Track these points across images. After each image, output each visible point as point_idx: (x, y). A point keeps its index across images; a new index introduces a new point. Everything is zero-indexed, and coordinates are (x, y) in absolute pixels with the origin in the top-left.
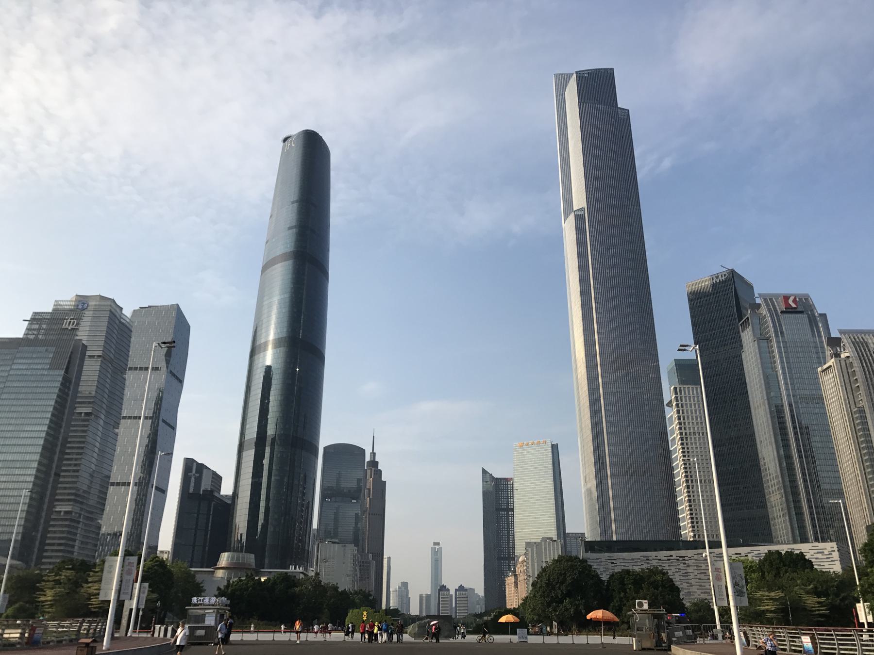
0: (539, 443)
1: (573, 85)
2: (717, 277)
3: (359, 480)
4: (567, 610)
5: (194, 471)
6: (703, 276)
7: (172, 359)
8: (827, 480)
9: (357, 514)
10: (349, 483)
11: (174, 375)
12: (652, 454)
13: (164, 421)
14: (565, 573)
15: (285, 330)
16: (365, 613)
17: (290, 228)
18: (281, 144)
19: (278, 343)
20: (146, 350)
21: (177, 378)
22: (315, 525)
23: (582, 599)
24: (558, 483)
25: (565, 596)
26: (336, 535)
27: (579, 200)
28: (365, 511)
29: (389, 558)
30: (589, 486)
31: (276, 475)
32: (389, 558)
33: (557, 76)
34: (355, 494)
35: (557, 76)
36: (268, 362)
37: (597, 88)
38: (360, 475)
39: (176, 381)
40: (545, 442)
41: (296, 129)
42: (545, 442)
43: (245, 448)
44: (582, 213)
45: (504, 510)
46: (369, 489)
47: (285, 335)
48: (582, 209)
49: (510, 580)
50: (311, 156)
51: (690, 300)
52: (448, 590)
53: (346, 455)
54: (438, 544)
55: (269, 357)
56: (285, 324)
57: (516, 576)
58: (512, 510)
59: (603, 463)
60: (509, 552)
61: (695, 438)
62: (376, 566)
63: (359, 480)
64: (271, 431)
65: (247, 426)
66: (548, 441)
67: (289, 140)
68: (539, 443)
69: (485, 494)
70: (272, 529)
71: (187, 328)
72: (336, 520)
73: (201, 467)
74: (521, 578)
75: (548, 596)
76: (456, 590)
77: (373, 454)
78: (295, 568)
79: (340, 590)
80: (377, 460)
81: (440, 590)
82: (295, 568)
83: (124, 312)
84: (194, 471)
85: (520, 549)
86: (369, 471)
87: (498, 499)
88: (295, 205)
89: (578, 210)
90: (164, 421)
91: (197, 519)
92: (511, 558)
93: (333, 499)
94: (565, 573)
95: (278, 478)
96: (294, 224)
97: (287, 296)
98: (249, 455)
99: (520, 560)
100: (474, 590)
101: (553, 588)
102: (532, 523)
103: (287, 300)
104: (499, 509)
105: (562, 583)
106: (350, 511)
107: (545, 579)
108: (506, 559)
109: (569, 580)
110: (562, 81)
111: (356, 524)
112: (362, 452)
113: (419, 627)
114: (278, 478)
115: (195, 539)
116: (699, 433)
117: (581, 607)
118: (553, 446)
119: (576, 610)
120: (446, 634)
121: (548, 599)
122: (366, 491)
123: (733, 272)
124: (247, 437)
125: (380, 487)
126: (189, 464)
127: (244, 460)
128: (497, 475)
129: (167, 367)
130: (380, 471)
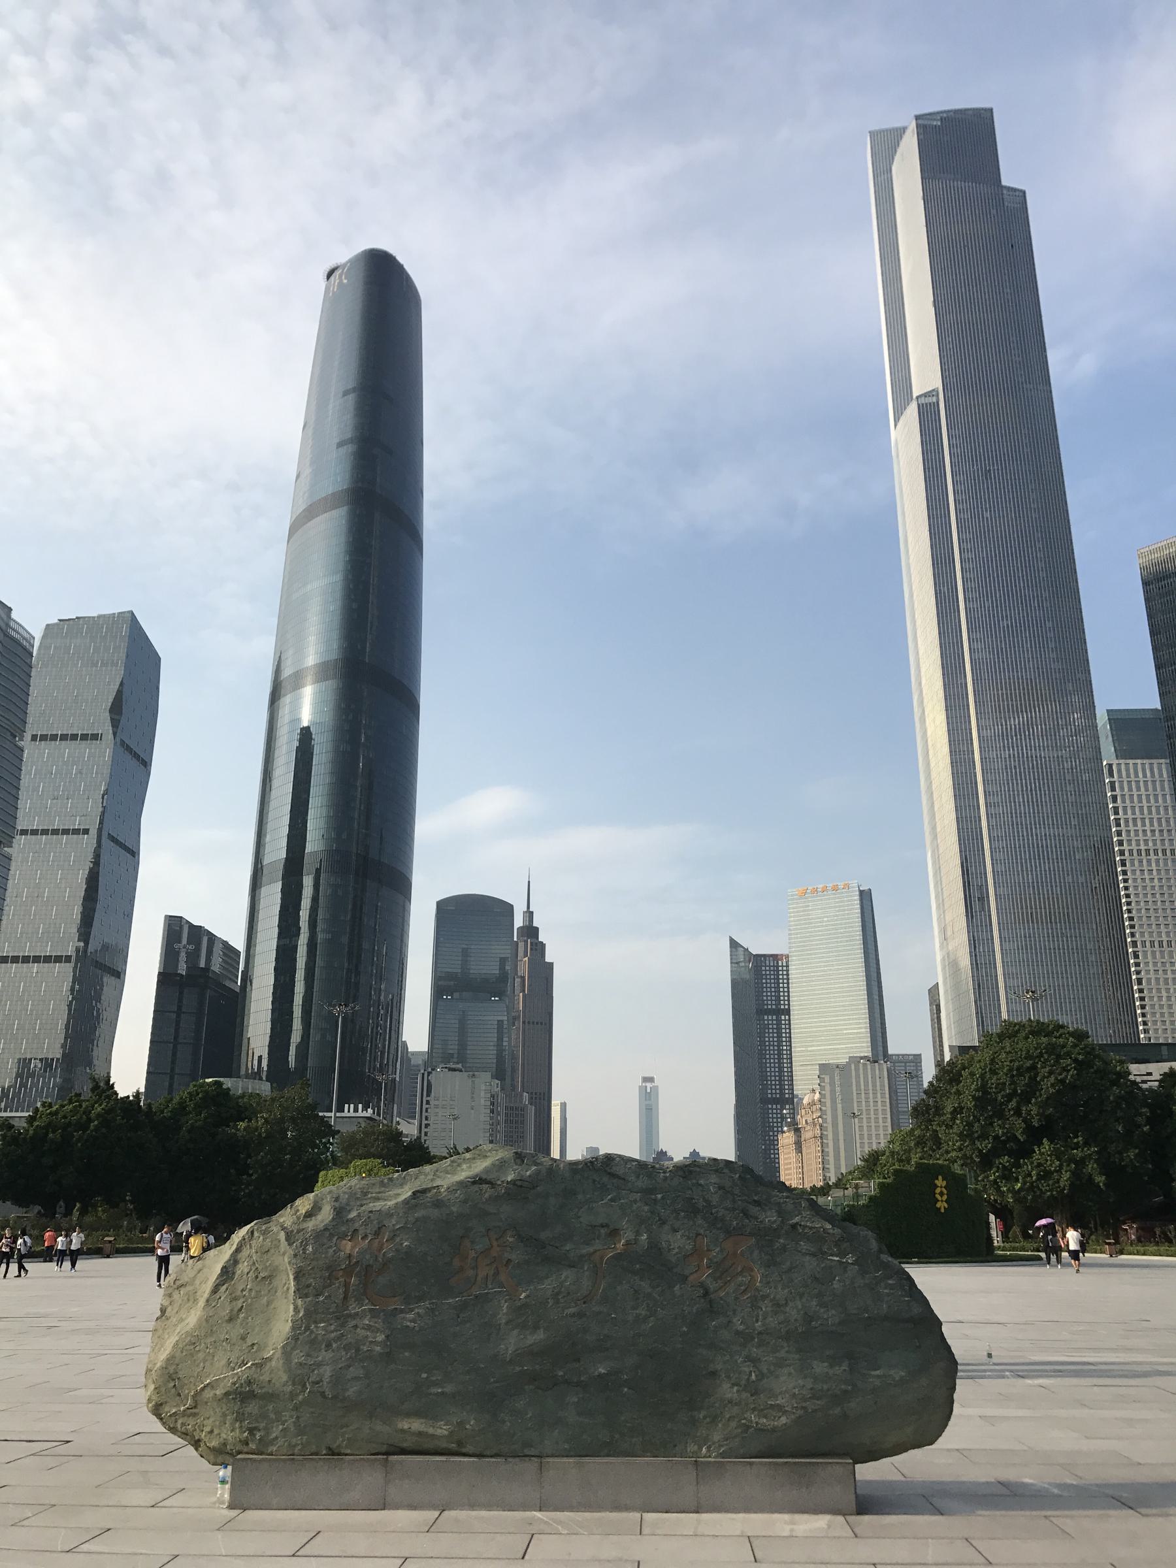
0: (835, 888)
1: (909, 146)
3: (503, 961)
4: (1046, 1175)
5: (184, 941)
7: (123, 720)
8: (874, 1141)
9: (500, 1022)
10: (485, 967)
11: (129, 749)
12: (1081, 879)
13: (113, 839)
14: (1034, 1067)
15: (335, 646)
16: (942, 1205)
18: (323, 284)
19: (323, 672)
20: (61, 699)
21: (136, 756)
23: (1086, 1143)
24: (872, 956)
25: (1035, 1135)
26: (462, 1059)
27: (926, 374)
28: (515, 1018)
29: (564, 1106)
30: (951, 946)
31: (323, 931)
32: (564, 1106)
36: (306, 719)
37: (959, 150)
38: (506, 952)
39: (134, 762)
40: (847, 886)
41: (345, 253)
42: (847, 886)
44: (934, 399)
45: (769, 1012)
46: (523, 978)
47: (334, 655)
49: (786, 1139)
50: (382, 307)
51: (1145, 583)
53: (472, 920)
54: (651, 1080)
55: (308, 706)
56: (335, 635)
57: (797, 1131)
59: (981, 899)
60: (782, 1089)
61: (1149, 861)
62: (538, 1114)
63: (503, 961)
64: (314, 842)
65: (268, 838)
66: (854, 884)
67: (337, 273)
68: (835, 888)
69: (735, 984)
70: (318, 1037)
71: (154, 661)
73: (197, 932)
74: (807, 1135)
75: (984, 1136)
77: (529, 914)
78: (356, 1110)
80: (535, 925)
82: (356, 1110)
83: (14, 615)
84: (184, 941)
85: (805, 1083)
87: (760, 996)
88: (351, 398)
89: (925, 395)
90: (113, 839)
91: (178, 1023)
92: (788, 1099)
93: (456, 995)
94: (1034, 1067)
96: (349, 435)
97: (338, 578)
98: (272, 895)
99: (805, 1101)
101: (1000, 1114)
102: (824, 1031)
103: (339, 587)
104: (762, 1012)
105: (1026, 1098)
106: (490, 1014)
107: (969, 1087)
108: (775, 1101)
109: (1048, 1086)
110: (885, 145)
111: (500, 1039)
112: (508, 909)
113: (336, 1281)
114: (329, 936)
115: (173, 1062)
116: (1156, 852)
117: (1091, 1167)
118: (861, 892)
119: (1075, 1174)
120: (789, 1388)
121: (986, 1145)
125: (543, 974)
126: (176, 928)
127: (263, 903)
128: (758, 946)
129: (115, 734)
130: (543, 945)
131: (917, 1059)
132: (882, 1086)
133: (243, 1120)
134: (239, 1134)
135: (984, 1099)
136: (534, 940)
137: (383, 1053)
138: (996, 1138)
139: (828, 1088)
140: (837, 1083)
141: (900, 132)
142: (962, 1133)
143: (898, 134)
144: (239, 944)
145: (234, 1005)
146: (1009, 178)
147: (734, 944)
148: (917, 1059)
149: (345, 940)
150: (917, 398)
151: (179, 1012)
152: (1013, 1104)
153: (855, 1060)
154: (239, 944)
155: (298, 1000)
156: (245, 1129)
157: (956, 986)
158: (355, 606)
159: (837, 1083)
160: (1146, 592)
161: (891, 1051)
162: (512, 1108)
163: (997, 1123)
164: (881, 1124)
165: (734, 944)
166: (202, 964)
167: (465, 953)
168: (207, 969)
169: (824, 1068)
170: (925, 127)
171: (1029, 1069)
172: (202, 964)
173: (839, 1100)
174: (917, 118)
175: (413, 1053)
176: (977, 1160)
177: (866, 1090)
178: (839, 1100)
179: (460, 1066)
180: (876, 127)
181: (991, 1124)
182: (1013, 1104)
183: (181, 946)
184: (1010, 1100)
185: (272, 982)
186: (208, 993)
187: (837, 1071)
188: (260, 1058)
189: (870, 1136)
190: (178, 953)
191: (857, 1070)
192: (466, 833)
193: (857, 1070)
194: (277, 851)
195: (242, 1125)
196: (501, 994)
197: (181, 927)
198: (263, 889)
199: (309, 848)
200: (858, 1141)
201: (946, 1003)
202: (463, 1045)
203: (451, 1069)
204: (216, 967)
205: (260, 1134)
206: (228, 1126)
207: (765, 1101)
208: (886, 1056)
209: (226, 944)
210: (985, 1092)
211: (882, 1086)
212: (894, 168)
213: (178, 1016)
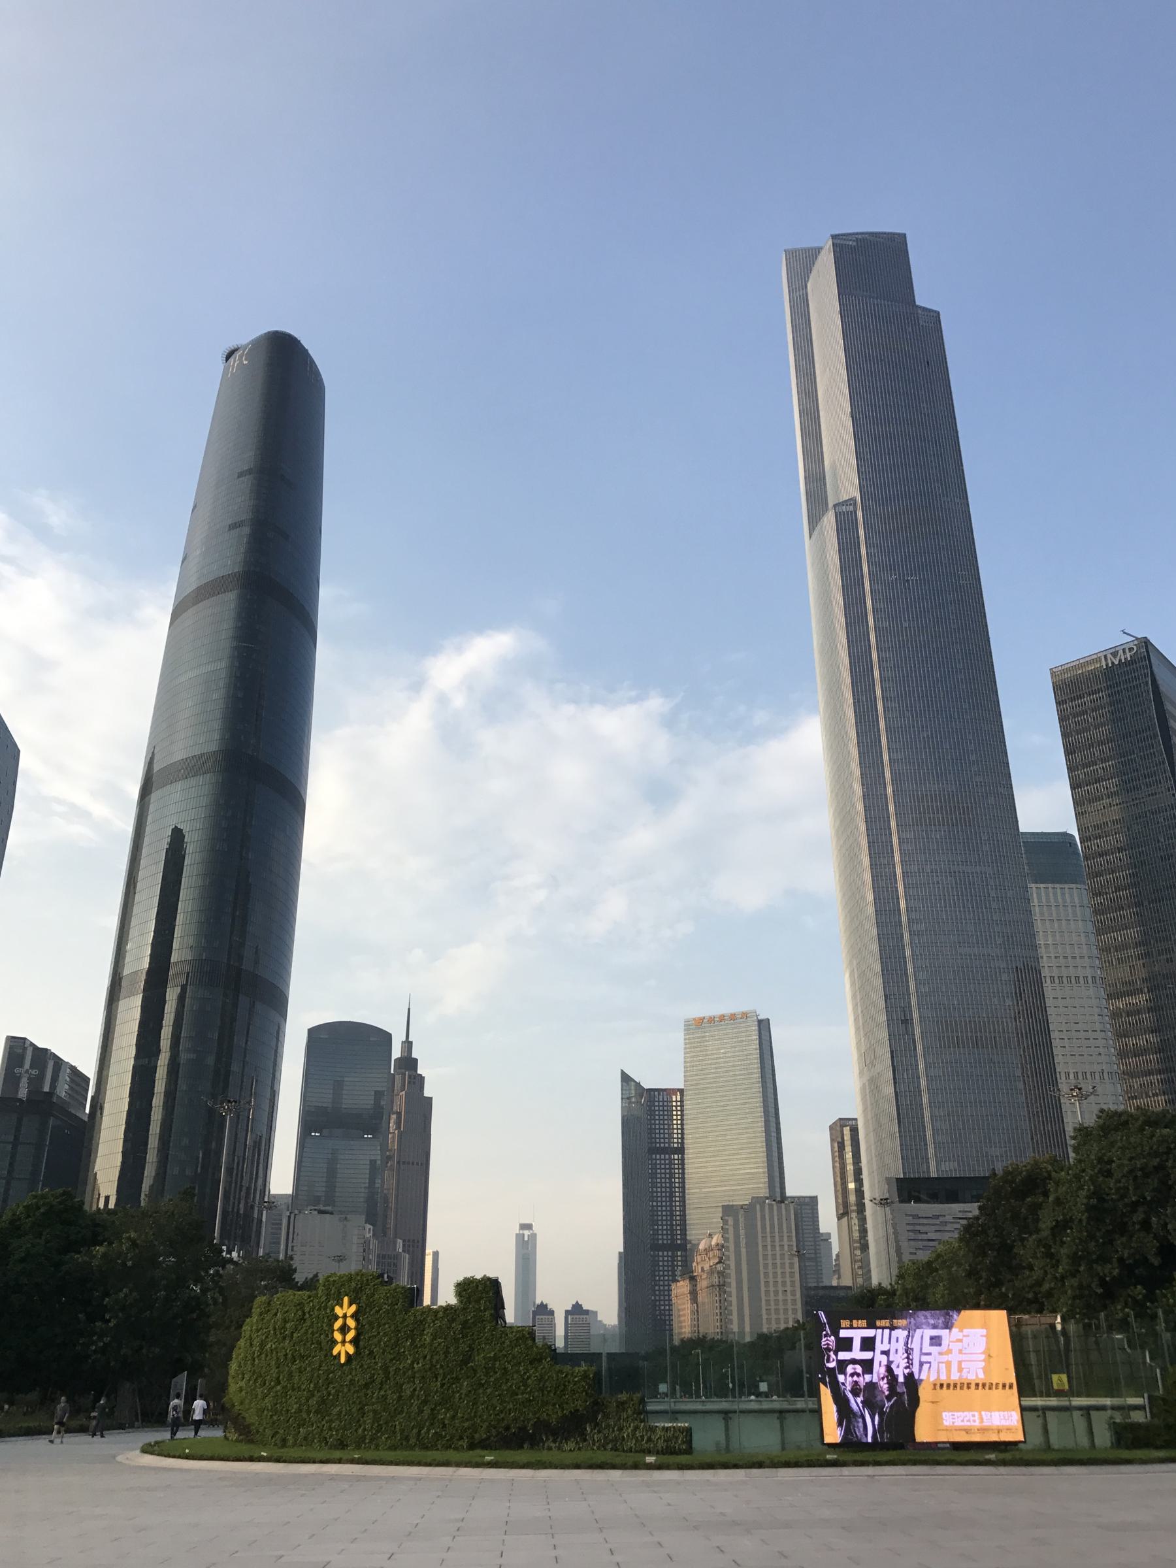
1: (826, 267)
2: (1115, 654)
3: (378, 1095)
5: (27, 1065)
6: (1094, 638)
17: (232, 527)
18: (220, 365)
22: (281, 1179)
27: (845, 484)
29: (436, 1255)
32: (436, 1255)
33: (791, 255)
34: (370, 1122)
35: (791, 255)
41: (249, 330)
43: (123, 991)
44: (851, 509)
46: (399, 1114)
47: (213, 747)
48: (852, 502)
49: (681, 1288)
52: (552, 1313)
53: (347, 1047)
54: (528, 1227)
57: (693, 1279)
58: (681, 1150)
62: (412, 1264)
63: (378, 1095)
64: (179, 953)
72: (332, 1174)
73: (43, 1056)
74: (703, 1283)
75: (1103, 1259)
76: (567, 1313)
77: (408, 1045)
79: (656, 703)
80: (414, 1055)
81: (535, 1313)
84: (27, 1065)
86: (398, 1078)
87: (651, 1132)
88: (247, 481)
93: (326, 1132)
95: (192, 1056)
98: (131, 1009)
99: (701, 1247)
100: (595, 1313)
102: (718, 1171)
106: (358, 1157)
110: (801, 263)
111: (372, 1181)
112: (387, 1037)
114: (192, 1056)
122: (394, 1117)
123: (1146, 642)
124: (127, 970)
125: (421, 1110)
127: (120, 1018)
130: (421, 1079)
131: (813, 1201)
132: (789, 1231)
133: (101, 1244)
134: (95, 1263)
135: (1099, 1209)
136: (412, 1073)
137: (248, 1193)
138: (1121, 1260)
139: (731, 1230)
140: (742, 1225)
141: (816, 252)
142: (1076, 1253)
143: (813, 254)
144: (89, 1069)
145: (82, 1136)
146: (923, 298)
147: (626, 1078)
148: (813, 1201)
149: (211, 1060)
150: (835, 506)
151: (15, 1144)
152: (1139, 1216)
153: (756, 1200)
154: (89, 1069)
155: (155, 1128)
156: (104, 1255)
157: (865, 1116)
158: (240, 695)
159: (742, 1225)
160: (1060, 712)
161: (790, 1192)
162: (384, 1257)
163: (1120, 1241)
164: (788, 1270)
165: (626, 1078)
166: (46, 1089)
167: (338, 1085)
168: (50, 1094)
169: (728, 1210)
170: (841, 246)
171: (1157, 1169)
172: (46, 1089)
173: (743, 1244)
174: (834, 237)
175: (275, 1196)
176: (1100, 1291)
177: (772, 1232)
178: (743, 1244)
179: (329, 1208)
180: (789, 247)
181: (1111, 1242)
182: (1139, 1216)
183: (23, 1070)
184: (1134, 1211)
185: (126, 1108)
186: (51, 1121)
187: (742, 1212)
188: (107, 1198)
189: (776, 1283)
190: (19, 1079)
191: (762, 1210)
192: (339, 963)
193: (762, 1210)
194: (140, 959)
195: (100, 1250)
196: (374, 1130)
197: (25, 1049)
198: (121, 1003)
199: (174, 958)
200: (763, 1289)
201: (867, 1135)
202: (331, 1186)
203: (321, 1212)
204: (63, 1090)
205: (124, 1264)
206: (79, 1253)
207: (656, 1247)
208: (784, 1198)
209: (74, 1069)
210: (1101, 1200)
211: (789, 1228)
212: (809, 285)
213: (15, 1147)
